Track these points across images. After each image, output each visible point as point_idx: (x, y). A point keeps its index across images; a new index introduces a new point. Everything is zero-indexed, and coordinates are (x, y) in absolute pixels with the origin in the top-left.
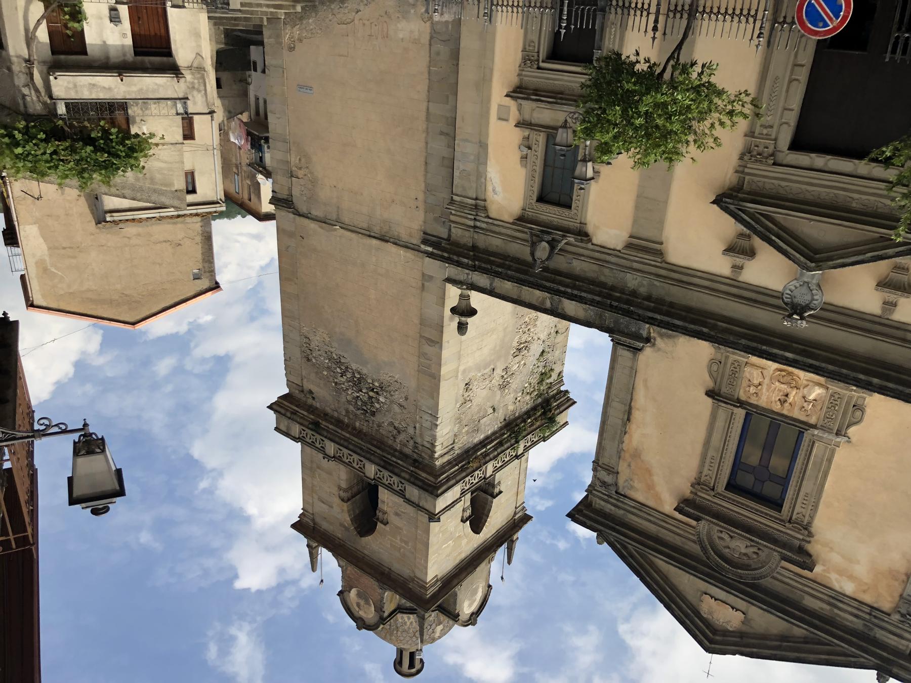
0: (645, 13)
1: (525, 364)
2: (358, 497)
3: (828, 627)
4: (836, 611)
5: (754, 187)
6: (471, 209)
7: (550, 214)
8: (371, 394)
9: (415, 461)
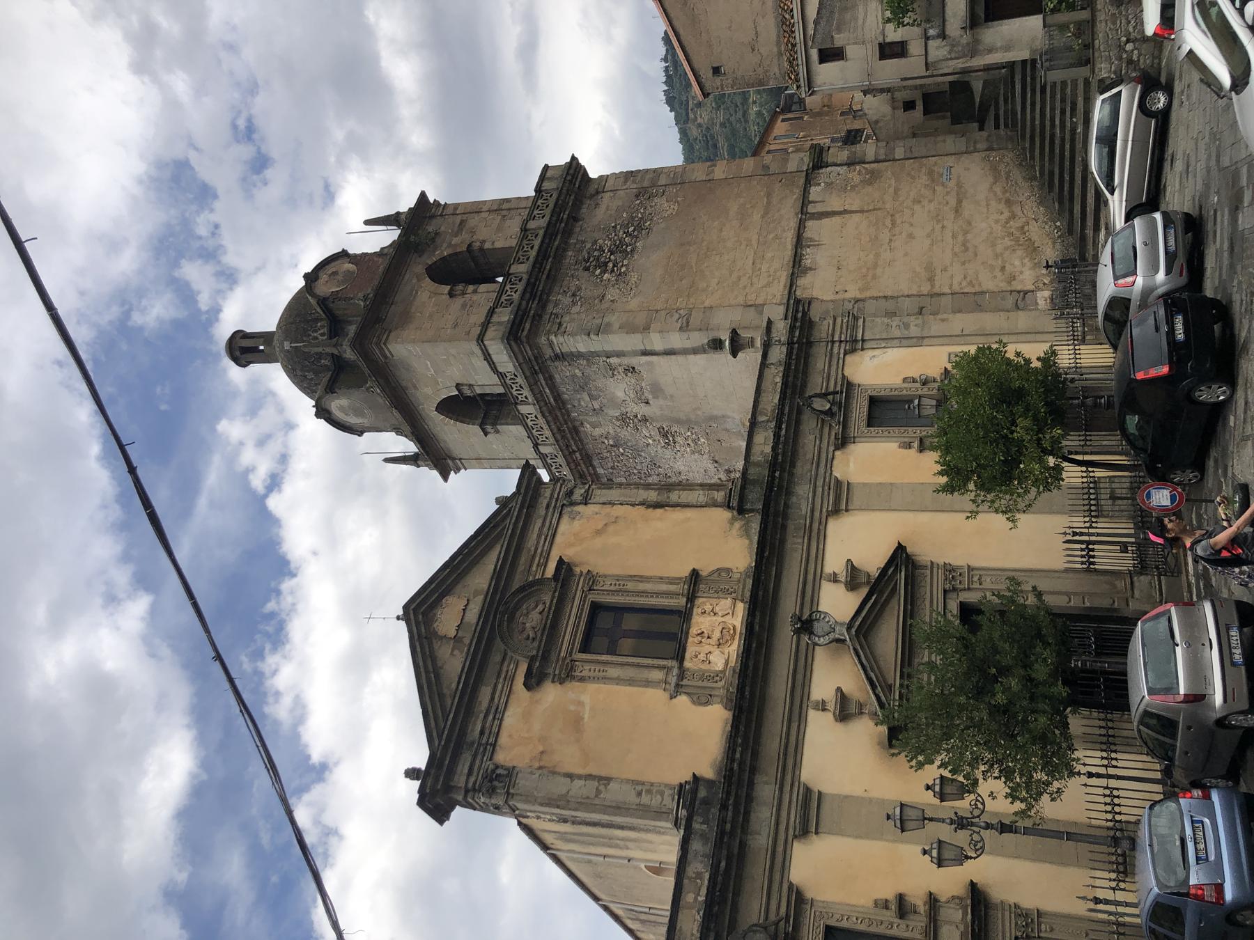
4: (482, 716)
6: (852, 336)
7: (860, 410)
8: (611, 265)
9: (540, 316)
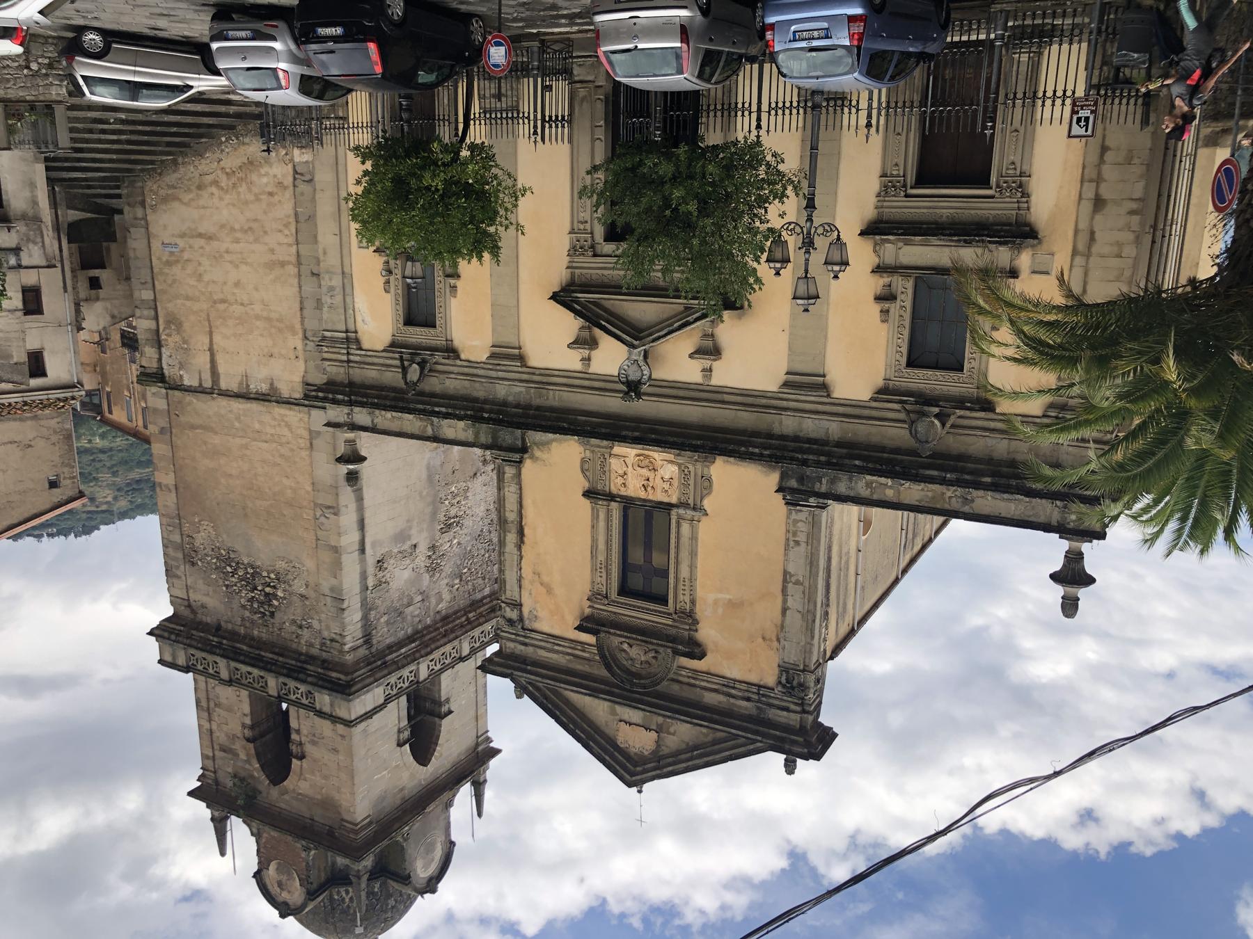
0: (746, 113)
1: (459, 543)
2: (269, 737)
3: (727, 720)
5: (583, 280)
7: (418, 335)
8: (268, 590)
9: (324, 661)
